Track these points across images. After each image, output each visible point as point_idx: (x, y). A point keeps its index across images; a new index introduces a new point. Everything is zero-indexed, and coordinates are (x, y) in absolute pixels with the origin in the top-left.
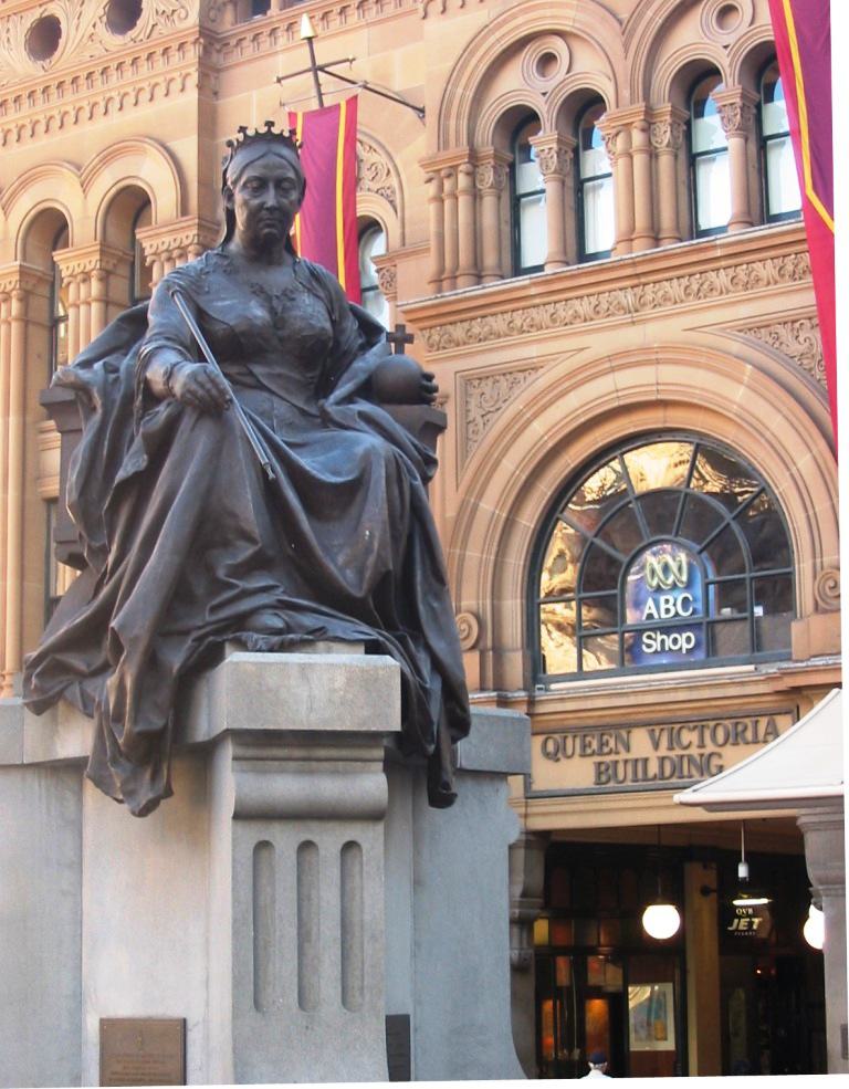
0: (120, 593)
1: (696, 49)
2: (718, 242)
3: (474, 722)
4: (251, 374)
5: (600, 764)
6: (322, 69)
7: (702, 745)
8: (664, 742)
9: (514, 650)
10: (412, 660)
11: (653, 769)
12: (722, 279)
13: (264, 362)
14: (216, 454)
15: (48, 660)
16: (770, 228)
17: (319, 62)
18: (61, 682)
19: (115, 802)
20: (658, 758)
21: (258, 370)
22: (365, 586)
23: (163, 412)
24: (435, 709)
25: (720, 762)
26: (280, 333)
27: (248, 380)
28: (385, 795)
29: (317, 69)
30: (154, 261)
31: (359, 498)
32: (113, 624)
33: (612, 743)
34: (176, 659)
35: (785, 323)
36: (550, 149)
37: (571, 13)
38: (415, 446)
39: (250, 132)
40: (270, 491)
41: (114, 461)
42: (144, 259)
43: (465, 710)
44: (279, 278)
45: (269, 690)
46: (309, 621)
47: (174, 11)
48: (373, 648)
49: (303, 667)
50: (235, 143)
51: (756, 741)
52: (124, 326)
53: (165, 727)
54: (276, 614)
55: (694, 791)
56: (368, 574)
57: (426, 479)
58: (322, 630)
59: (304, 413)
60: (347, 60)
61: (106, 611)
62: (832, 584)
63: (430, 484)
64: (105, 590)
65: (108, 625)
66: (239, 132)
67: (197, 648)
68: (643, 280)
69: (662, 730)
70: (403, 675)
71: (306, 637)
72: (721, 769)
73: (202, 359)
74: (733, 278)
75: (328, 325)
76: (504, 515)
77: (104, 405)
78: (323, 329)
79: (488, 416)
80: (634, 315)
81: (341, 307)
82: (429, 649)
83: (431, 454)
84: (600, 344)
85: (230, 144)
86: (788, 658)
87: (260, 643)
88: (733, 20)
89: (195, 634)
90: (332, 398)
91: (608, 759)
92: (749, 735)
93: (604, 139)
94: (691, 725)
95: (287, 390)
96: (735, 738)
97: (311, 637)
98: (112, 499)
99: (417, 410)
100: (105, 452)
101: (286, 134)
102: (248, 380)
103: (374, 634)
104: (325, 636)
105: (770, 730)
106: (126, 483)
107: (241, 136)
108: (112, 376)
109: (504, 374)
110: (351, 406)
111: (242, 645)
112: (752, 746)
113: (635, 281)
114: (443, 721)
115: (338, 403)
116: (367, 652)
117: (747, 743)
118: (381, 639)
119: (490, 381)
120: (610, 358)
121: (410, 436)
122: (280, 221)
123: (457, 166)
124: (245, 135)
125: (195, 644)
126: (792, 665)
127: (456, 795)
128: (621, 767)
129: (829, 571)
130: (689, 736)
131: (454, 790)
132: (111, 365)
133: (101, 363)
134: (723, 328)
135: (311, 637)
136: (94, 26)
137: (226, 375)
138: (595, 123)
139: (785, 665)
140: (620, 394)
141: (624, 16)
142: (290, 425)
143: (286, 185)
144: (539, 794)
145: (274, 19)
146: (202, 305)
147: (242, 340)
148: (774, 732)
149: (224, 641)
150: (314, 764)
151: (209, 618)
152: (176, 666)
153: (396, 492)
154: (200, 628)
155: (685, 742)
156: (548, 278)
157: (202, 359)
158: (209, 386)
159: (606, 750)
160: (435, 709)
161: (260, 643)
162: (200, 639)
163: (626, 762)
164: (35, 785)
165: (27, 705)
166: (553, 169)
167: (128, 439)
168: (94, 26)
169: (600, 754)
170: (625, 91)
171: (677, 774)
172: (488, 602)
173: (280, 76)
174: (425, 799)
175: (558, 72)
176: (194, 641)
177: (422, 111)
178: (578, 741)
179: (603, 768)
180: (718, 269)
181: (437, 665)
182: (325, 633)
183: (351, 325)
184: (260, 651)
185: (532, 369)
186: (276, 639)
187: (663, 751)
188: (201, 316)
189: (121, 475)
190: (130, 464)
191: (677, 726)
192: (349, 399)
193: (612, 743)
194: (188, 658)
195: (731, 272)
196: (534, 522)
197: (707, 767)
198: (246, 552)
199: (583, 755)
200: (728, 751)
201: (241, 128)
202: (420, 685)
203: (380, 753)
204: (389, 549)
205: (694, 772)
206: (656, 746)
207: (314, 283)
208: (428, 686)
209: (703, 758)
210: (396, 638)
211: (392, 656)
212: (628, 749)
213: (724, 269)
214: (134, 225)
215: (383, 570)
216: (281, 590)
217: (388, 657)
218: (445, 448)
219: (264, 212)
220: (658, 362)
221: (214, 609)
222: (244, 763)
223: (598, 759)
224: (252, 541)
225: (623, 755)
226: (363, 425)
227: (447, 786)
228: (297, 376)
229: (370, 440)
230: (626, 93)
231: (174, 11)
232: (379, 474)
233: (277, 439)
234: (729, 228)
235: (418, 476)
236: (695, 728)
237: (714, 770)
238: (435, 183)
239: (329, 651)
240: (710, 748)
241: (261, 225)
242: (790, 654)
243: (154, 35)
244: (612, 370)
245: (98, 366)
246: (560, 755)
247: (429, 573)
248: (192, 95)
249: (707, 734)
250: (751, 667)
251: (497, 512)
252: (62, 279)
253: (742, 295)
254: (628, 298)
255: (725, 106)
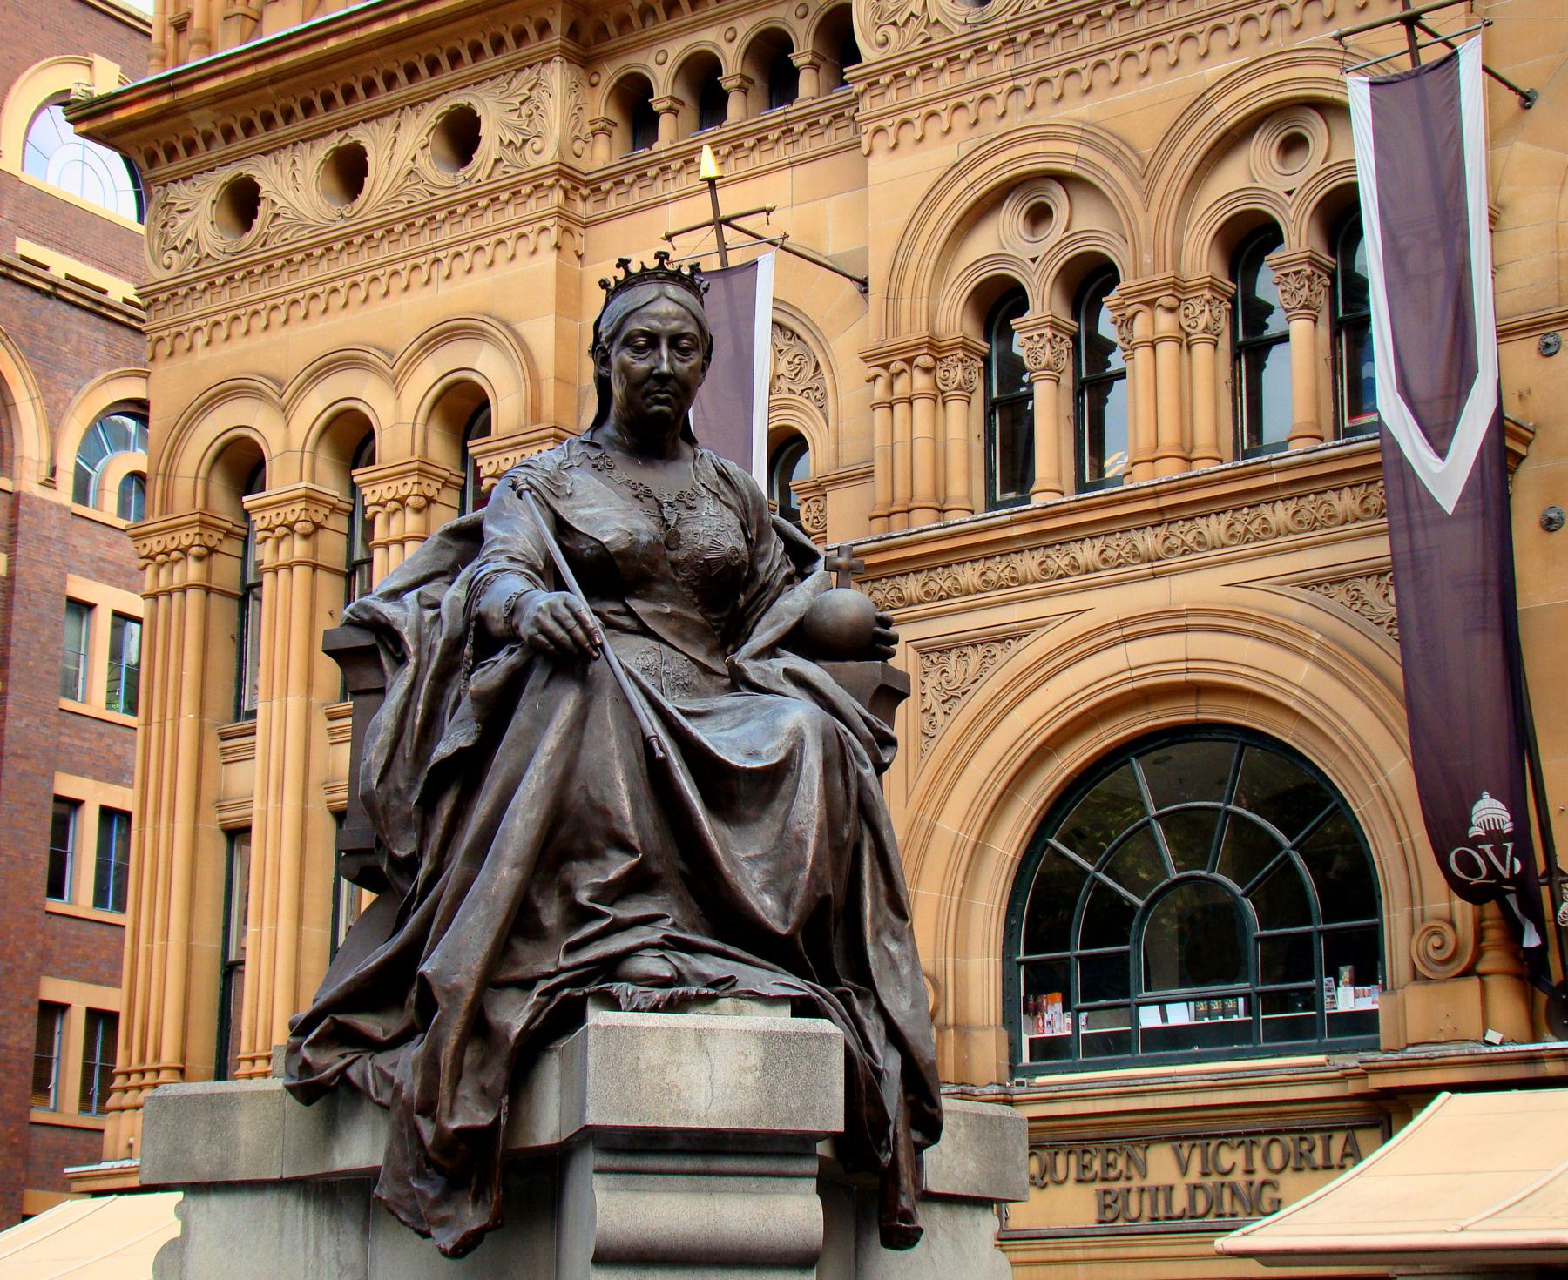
0: (433, 928)
1: (1247, 197)
2: (1274, 464)
3: (948, 1121)
4: (631, 613)
5: (1106, 1192)
6: (727, 221)
7: (1249, 1172)
8: (1196, 1165)
9: (985, 1028)
10: (857, 1026)
11: (1180, 1202)
12: (1279, 514)
13: (645, 597)
14: (580, 721)
15: (326, 1021)
16: (1347, 444)
17: (725, 212)
18: (343, 1056)
19: (417, 1237)
20: (1188, 1186)
21: (637, 605)
22: (793, 918)
23: (504, 660)
24: (893, 1097)
25: (1278, 1195)
26: (673, 555)
27: (626, 621)
28: (819, 1228)
29: (721, 222)
30: (493, 485)
31: (785, 788)
32: (426, 968)
33: (1121, 1164)
34: (514, 1015)
35: (1369, 577)
36: (1041, 336)
37: (1072, 148)
38: (865, 719)
39: (635, 268)
40: (656, 775)
41: (431, 728)
42: (478, 481)
43: (935, 1104)
44: (665, 480)
45: (650, 1068)
46: (712, 967)
47: (525, 142)
48: (803, 1008)
49: (700, 1035)
50: (613, 284)
51: (1328, 1167)
52: (449, 542)
53: (497, 1119)
54: (662, 957)
55: (1244, 1234)
56: (798, 900)
57: (881, 768)
58: (729, 981)
59: (706, 670)
60: (763, 210)
61: (414, 951)
62: (1437, 944)
63: (885, 775)
64: (413, 920)
65: (415, 969)
66: (618, 266)
67: (546, 1005)
68: (1168, 516)
69: (1194, 1145)
70: (847, 1049)
71: (705, 991)
72: (1277, 1204)
73: (560, 585)
74: (1295, 513)
75: (742, 545)
76: (972, 840)
77: (418, 652)
78: (735, 550)
79: (951, 702)
80: (1155, 568)
81: (761, 522)
82: (882, 1011)
83: (888, 730)
84: (1110, 604)
85: (604, 284)
86: (1375, 1047)
87: (638, 999)
88: (1296, 159)
89: (543, 985)
90: (745, 650)
91: (1117, 1186)
92: (1318, 1156)
93: (1115, 323)
94: (1236, 1141)
95: (681, 636)
96: (1300, 1162)
97: (712, 991)
98: (425, 789)
99: (869, 669)
100: (418, 721)
101: (686, 272)
102: (626, 621)
103: (800, 987)
104: (733, 990)
105: (1348, 1150)
106: (445, 762)
107: (621, 274)
108: (429, 614)
109: (974, 646)
110: (773, 661)
111: (613, 1003)
112: (1321, 1174)
113: (1157, 519)
114: (900, 1120)
115: (758, 655)
116: (794, 1015)
117: (1315, 1169)
118: (816, 995)
119: (953, 655)
120: (1121, 624)
121: (858, 705)
122: (675, 395)
123: (914, 358)
124: (627, 272)
125: (543, 999)
126: (1380, 1057)
127: (920, 1230)
128: (1133, 1199)
129: (1433, 923)
130: (1230, 1157)
131: (920, 1223)
132: (428, 597)
133: (414, 593)
134: (1281, 582)
135: (712, 991)
136: (414, 159)
137: (596, 613)
138: (1104, 299)
139: (1369, 1056)
140: (1191, 665)
141: (1147, 152)
142: (687, 688)
143: (685, 343)
144: (1016, 1235)
145: (663, 155)
146: (567, 517)
147: (619, 563)
148: (1353, 1155)
149: (586, 995)
150: (714, 1181)
151: (565, 962)
152: (516, 1029)
153: (839, 783)
154: (549, 976)
155: (1226, 1165)
156: (1036, 512)
157: (560, 585)
158: (572, 623)
159: (1112, 1173)
160: (893, 1097)
161: (638, 999)
162: (549, 993)
163: (1142, 1190)
164: (295, 1213)
165: (290, 1089)
166: (1043, 364)
167: (452, 699)
168: (414, 159)
169: (1104, 1179)
170: (1145, 256)
171: (1214, 1210)
172: (950, 959)
173: (671, 231)
174: (875, 1238)
175: (1055, 231)
176: (540, 994)
177: (864, 283)
178: (1073, 1159)
179: (1109, 1199)
180: (1274, 502)
181: (895, 1036)
182: (734, 985)
183: (776, 547)
184: (636, 1010)
185: (1013, 639)
186: (658, 994)
187: (1194, 1176)
188: (562, 528)
189: (443, 750)
190: (455, 737)
191: (1214, 1143)
192: (770, 651)
193: (1121, 1164)
194: (531, 1020)
195: (1292, 505)
196: (1014, 849)
197: (1259, 1202)
198: (618, 866)
199: (1079, 1181)
200: (1288, 1180)
201: (620, 260)
202: (870, 1064)
203: (812, 1166)
204: (827, 865)
205: (1238, 1208)
206: (1184, 1170)
207: (722, 486)
208: (881, 1066)
209: (1254, 1188)
210: (838, 995)
211: (832, 1020)
212: (1144, 1176)
213: (1283, 500)
214: (466, 437)
215: (819, 895)
216: (670, 921)
217: (825, 1021)
218: (905, 720)
219: (651, 381)
220: (1188, 629)
221: (572, 948)
222: (611, 1177)
223: (1105, 1186)
224: (626, 847)
225: (1136, 1183)
226: (789, 688)
227: (908, 1216)
228: (697, 617)
229: (799, 713)
230: (1147, 259)
231: (525, 142)
232: (812, 761)
233: (669, 706)
234: (1291, 444)
235: (869, 762)
236: (1242, 1143)
237: (1266, 1206)
238: (881, 383)
239: (739, 1012)
240: (1261, 1175)
241: (649, 400)
242: (1378, 1040)
243: (497, 175)
244: (1125, 640)
245: (411, 597)
246: (1047, 1179)
247: (883, 900)
248: (548, 259)
249: (1257, 1154)
250: (1321, 1058)
251: (962, 834)
252: (365, 509)
253: (1307, 537)
254: (1148, 541)
255: (1286, 275)
